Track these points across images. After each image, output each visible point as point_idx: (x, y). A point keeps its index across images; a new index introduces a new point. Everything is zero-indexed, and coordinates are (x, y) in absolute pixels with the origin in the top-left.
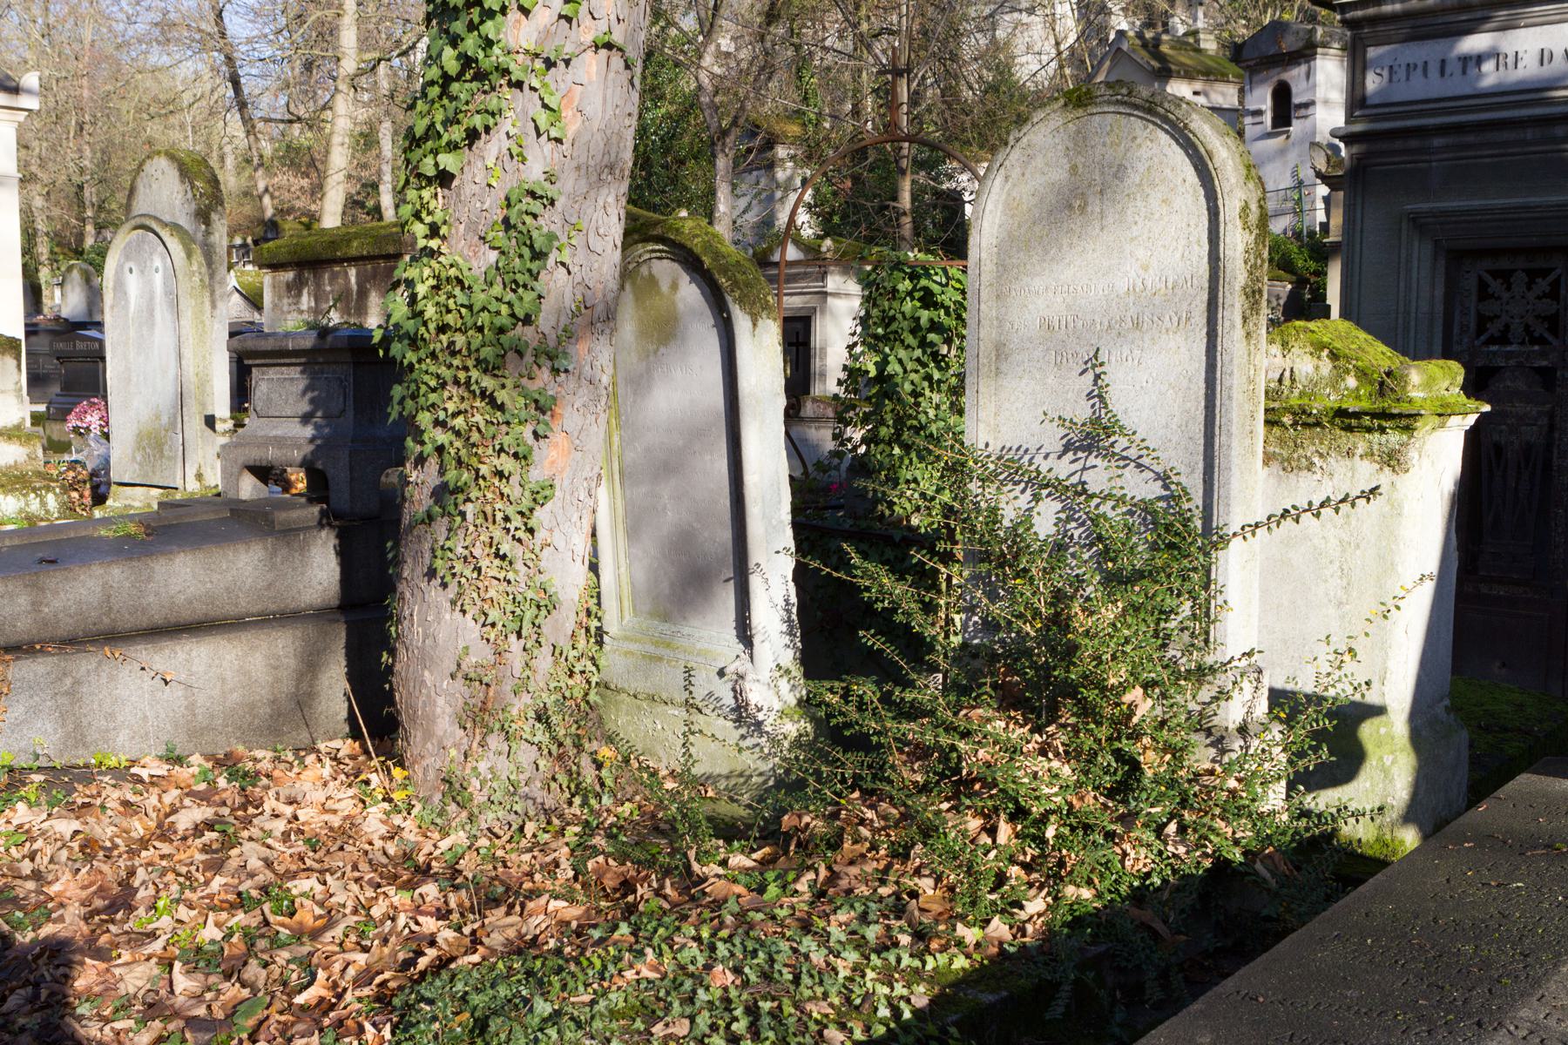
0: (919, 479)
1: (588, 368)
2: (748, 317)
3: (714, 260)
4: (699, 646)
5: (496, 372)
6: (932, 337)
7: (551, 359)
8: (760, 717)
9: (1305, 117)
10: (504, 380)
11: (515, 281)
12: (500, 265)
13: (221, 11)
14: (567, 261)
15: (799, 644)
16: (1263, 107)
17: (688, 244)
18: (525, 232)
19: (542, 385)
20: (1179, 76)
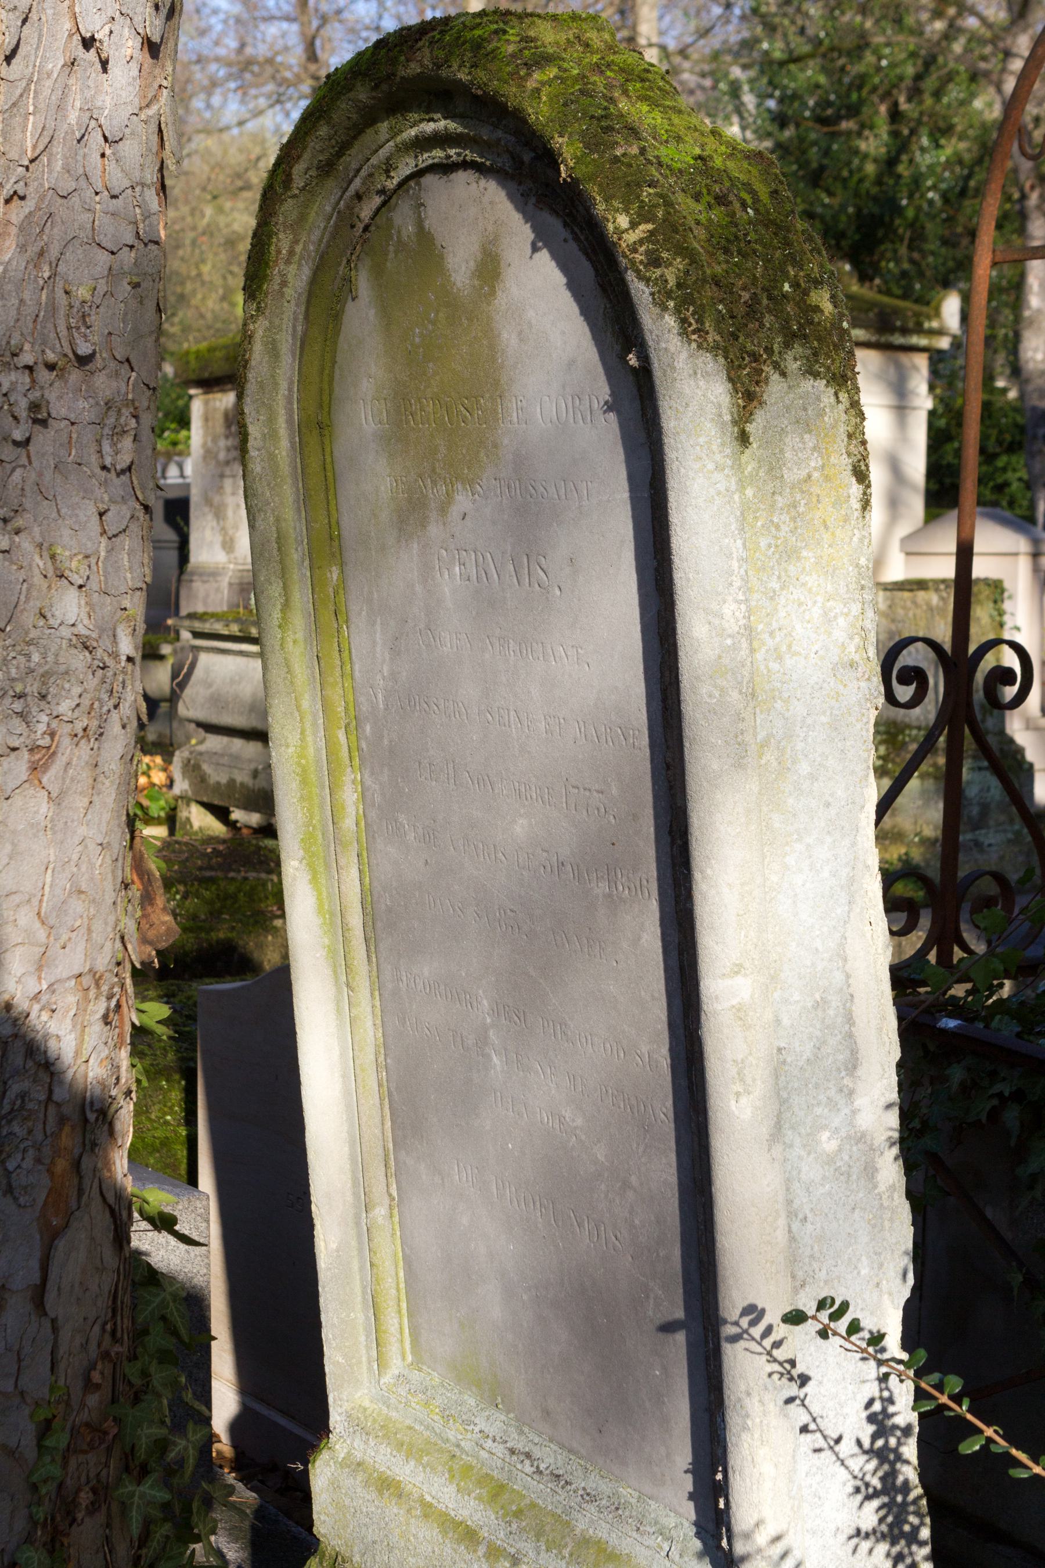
2: (711, 365)
3: (593, 143)
13: (314, 38)
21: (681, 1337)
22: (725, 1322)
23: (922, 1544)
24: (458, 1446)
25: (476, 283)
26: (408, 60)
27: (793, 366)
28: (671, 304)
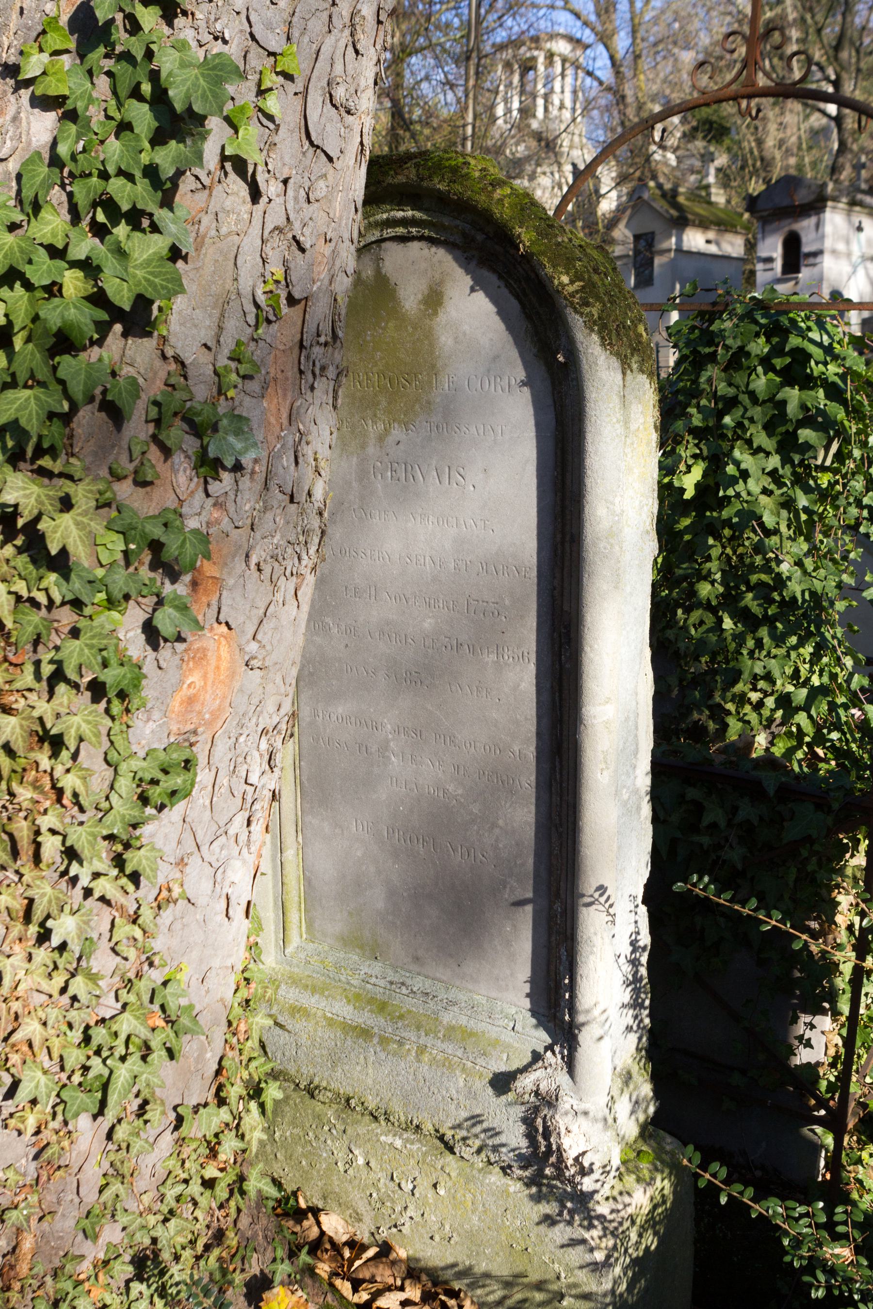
0: (776, 673)
1: (287, 460)
2: (615, 363)
4: (447, 1018)
5: (46, 462)
6: (806, 434)
7: (196, 429)
8: (587, 1184)
9: (814, 265)
10: (68, 487)
11: (108, 204)
12: (63, 150)
14: (253, 156)
15: (647, 1021)
16: (775, 255)
17: (482, 200)
18: (139, 54)
19: (171, 502)
20: (694, 225)
21: (529, 908)
22: (583, 895)
23: (645, 1008)
24: (348, 983)
25: (422, 307)
26: (396, 174)
27: (635, 366)
28: (596, 328)
